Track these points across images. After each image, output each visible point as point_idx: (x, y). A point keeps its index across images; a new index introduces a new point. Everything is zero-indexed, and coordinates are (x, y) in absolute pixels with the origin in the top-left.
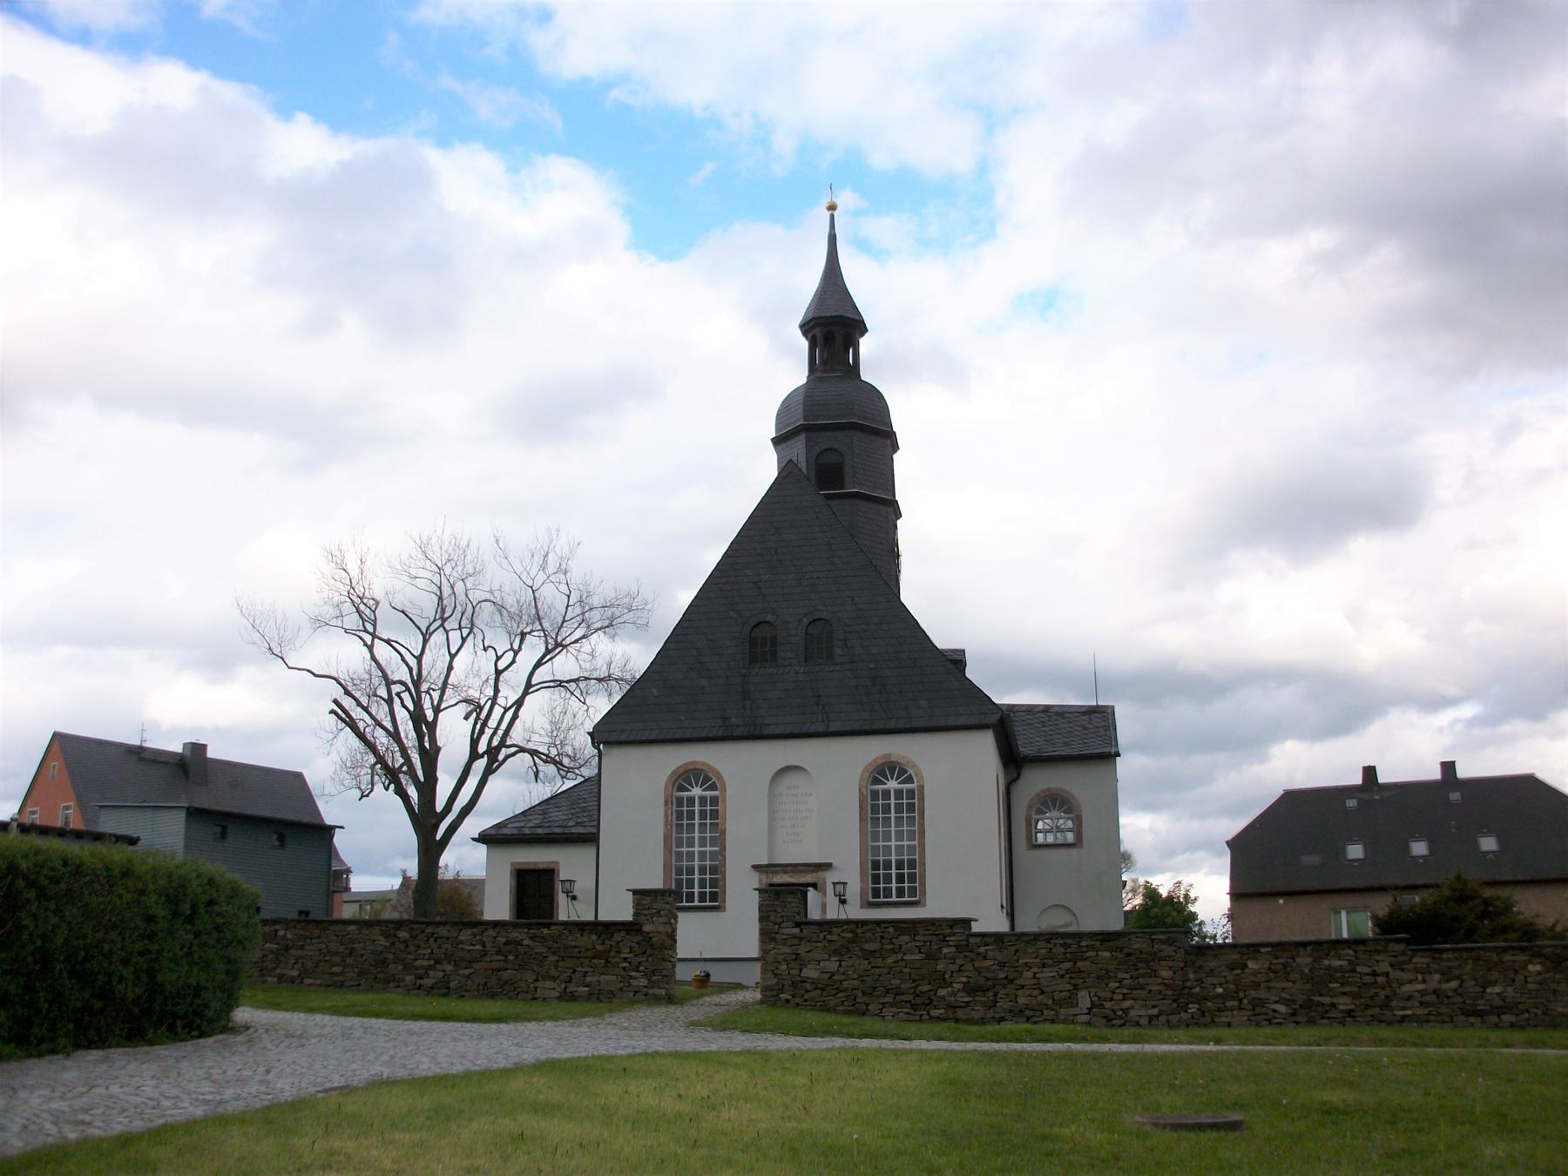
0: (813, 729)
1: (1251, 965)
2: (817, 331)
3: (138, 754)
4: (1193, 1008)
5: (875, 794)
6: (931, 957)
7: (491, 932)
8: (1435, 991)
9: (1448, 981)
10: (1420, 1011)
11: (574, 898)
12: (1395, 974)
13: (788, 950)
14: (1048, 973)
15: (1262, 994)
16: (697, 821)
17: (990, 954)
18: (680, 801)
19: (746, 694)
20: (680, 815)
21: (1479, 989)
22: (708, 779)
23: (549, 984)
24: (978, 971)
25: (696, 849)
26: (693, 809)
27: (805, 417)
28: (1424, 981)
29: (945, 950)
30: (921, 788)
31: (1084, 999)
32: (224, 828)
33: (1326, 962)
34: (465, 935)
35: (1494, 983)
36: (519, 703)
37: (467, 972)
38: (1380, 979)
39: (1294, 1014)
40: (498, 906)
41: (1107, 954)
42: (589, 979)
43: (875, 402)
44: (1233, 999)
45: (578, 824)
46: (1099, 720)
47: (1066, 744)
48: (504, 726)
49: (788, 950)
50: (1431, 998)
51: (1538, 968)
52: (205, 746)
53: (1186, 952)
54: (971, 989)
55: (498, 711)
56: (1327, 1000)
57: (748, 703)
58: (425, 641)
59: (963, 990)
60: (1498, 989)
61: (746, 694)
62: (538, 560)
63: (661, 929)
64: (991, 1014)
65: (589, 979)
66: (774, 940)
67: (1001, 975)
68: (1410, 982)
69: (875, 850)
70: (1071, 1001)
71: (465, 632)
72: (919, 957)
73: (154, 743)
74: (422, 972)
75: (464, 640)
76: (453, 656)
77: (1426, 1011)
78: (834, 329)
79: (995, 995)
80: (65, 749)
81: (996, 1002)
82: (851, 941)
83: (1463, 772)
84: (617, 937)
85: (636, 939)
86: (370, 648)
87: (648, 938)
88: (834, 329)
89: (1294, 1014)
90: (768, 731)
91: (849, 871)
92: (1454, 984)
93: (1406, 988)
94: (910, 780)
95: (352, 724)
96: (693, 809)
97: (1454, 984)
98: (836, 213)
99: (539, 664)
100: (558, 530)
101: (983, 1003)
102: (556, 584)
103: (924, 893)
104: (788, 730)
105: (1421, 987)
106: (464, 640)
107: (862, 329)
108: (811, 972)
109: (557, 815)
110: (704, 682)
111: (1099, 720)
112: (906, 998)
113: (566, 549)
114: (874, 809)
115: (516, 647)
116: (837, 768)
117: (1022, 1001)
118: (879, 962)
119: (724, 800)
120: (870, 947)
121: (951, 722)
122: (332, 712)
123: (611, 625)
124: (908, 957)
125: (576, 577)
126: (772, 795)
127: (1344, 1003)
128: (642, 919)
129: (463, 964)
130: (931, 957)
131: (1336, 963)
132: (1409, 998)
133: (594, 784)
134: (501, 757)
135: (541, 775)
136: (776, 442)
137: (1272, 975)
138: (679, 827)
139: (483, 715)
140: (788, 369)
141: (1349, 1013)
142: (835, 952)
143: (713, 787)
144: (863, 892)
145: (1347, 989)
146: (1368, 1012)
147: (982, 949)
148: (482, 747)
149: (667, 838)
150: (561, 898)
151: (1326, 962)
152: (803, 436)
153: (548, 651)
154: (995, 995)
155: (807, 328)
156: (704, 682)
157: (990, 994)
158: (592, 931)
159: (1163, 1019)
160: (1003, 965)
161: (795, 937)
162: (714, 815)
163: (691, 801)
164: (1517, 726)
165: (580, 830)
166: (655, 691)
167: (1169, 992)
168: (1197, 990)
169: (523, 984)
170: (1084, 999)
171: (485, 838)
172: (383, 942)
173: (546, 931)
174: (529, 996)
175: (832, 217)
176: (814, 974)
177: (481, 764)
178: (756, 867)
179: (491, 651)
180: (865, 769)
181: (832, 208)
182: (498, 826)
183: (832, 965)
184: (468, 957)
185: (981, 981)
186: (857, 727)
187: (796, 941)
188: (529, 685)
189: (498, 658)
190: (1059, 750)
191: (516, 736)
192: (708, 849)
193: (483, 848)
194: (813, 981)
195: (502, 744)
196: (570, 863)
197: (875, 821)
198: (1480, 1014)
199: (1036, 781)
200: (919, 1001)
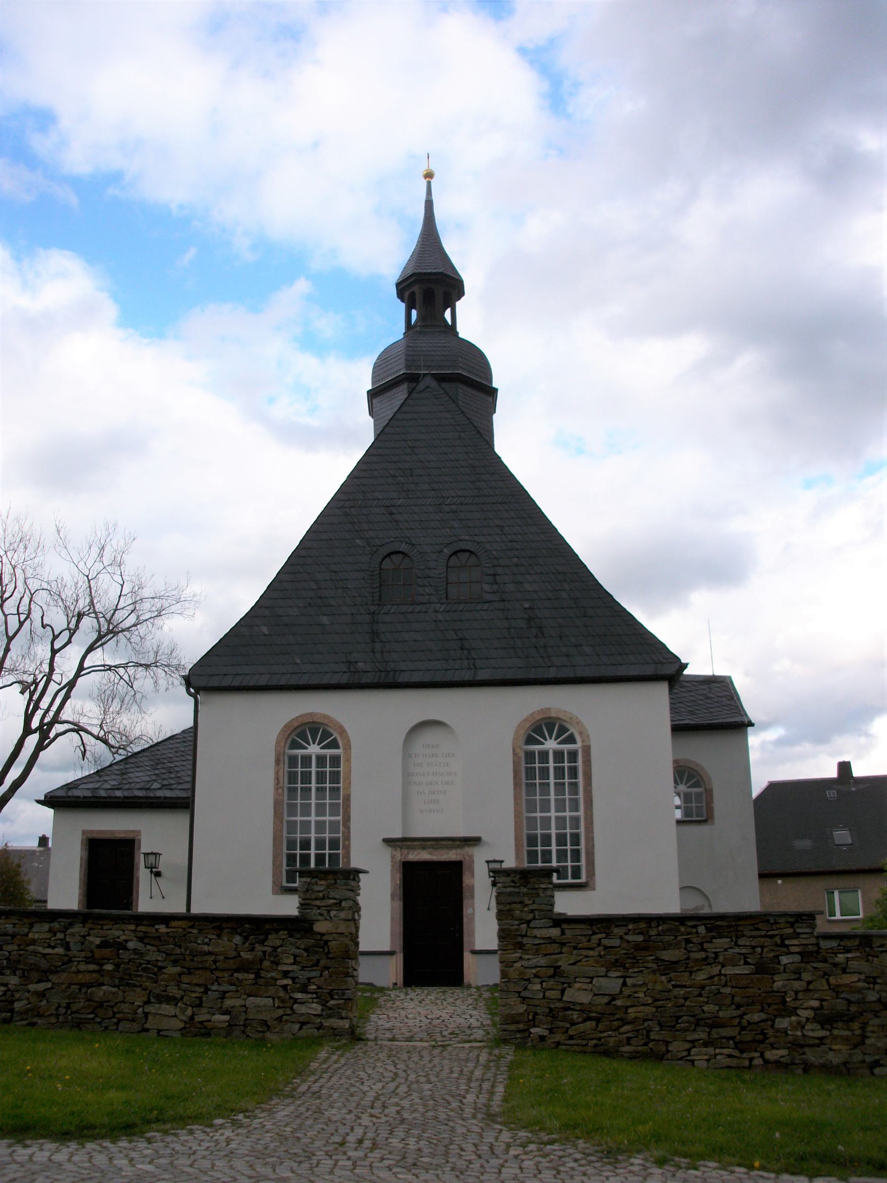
0: (457, 677)
2: (416, 289)
5: (530, 756)
6: (764, 969)
7: (78, 929)
11: (158, 874)
13: (542, 961)
16: (313, 785)
17: (854, 964)
18: (293, 760)
19: (375, 635)
20: (292, 778)
22: (326, 734)
24: (836, 990)
25: (313, 818)
26: (310, 767)
27: (408, 367)
29: (784, 960)
30: (587, 750)
34: (40, 931)
36: (71, 684)
37: (41, 987)
40: (64, 891)
42: (228, 1003)
43: (476, 360)
45: (163, 787)
47: (692, 713)
48: (54, 708)
49: (542, 961)
54: (825, 1019)
55: (53, 688)
57: (378, 646)
59: (815, 1019)
61: (375, 635)
62: (95, 551)
63: (342, 929)
64: (858, 1056)
65: (228, 1003)
66: (521, 946)
67: (872, 996)
69: (532, 822)
71: (23, 617)
72: (746, 970)
75: (21, 624)
76: (10, 639)
79: (863, 1027)
81: (864, 1037)
82: (637, 947)
83: (858, 771)
84: (274, 940)
85: (303, 943)
87: (322, 942)
90: (404, 678)
94: (571, 740)
96: (310, 767)
98: (433, 182)
99: (91, 649)
100: (115, 525)
101: (846, 1040)
102: (112, 574)
103: (591, 873)
104: (427, 678)
106: (21, 624)
108: (578, 994)
109: (140, 776)
110: (325, 620)
112: (724, 1032)
113: (122, 543)
114: (530, 771)
115: (72, 625)
116: (487, 723)
118: (685, 979)
119: (348, 760)
120: (669, 955)
121: (622, 671)
123: (159, 615)
124: (729, 971)
125: (129, 569)
126: (407, 755)
128: (313, 913)
129: (35, 975)
130: (764, 969)
133: (188, 740)
134: (52, 735)
135: (88, 754)
136: (372, 395)
138: (292, 791)
139: (35, 697)
142: (616, 964)
143: (334, 745)
147: (841, 958)
148: (35, 723)
149: (277, 804)
150: (143, 875)
153: (100, 637)
154: (863, 1027)
156: (325, 620)
157: (856, 1025)
158: (234, 931)
160: (871, 980)
161: (551, 940)
162: (335, 777)
163: (306, 760)
164: (807, 747)
165: (168, 793)
166: (265, 630)
169: (125, 1007)
171: (51, 801)
173: (163, 929)
174: (136, 1027)
175: (429, 184)
176: (585, 998)
177: (32, 740)
179: (48, 628)
180: (519, 726)
181: (429, 175)
182: (68, 786)
183: (612, 984)
184: (44, 964)
185: (840, 1005)
186: (510, 675)
187: (555, 948)
188: (81, 667)
189: (55, 637)
191: (65, 715)
192: (327, 818)
193: (50, 812)
194: (583, 1009)
195: (56, 720)
196: (155, 833)
197: (531, 787)
200: (747, 1036)
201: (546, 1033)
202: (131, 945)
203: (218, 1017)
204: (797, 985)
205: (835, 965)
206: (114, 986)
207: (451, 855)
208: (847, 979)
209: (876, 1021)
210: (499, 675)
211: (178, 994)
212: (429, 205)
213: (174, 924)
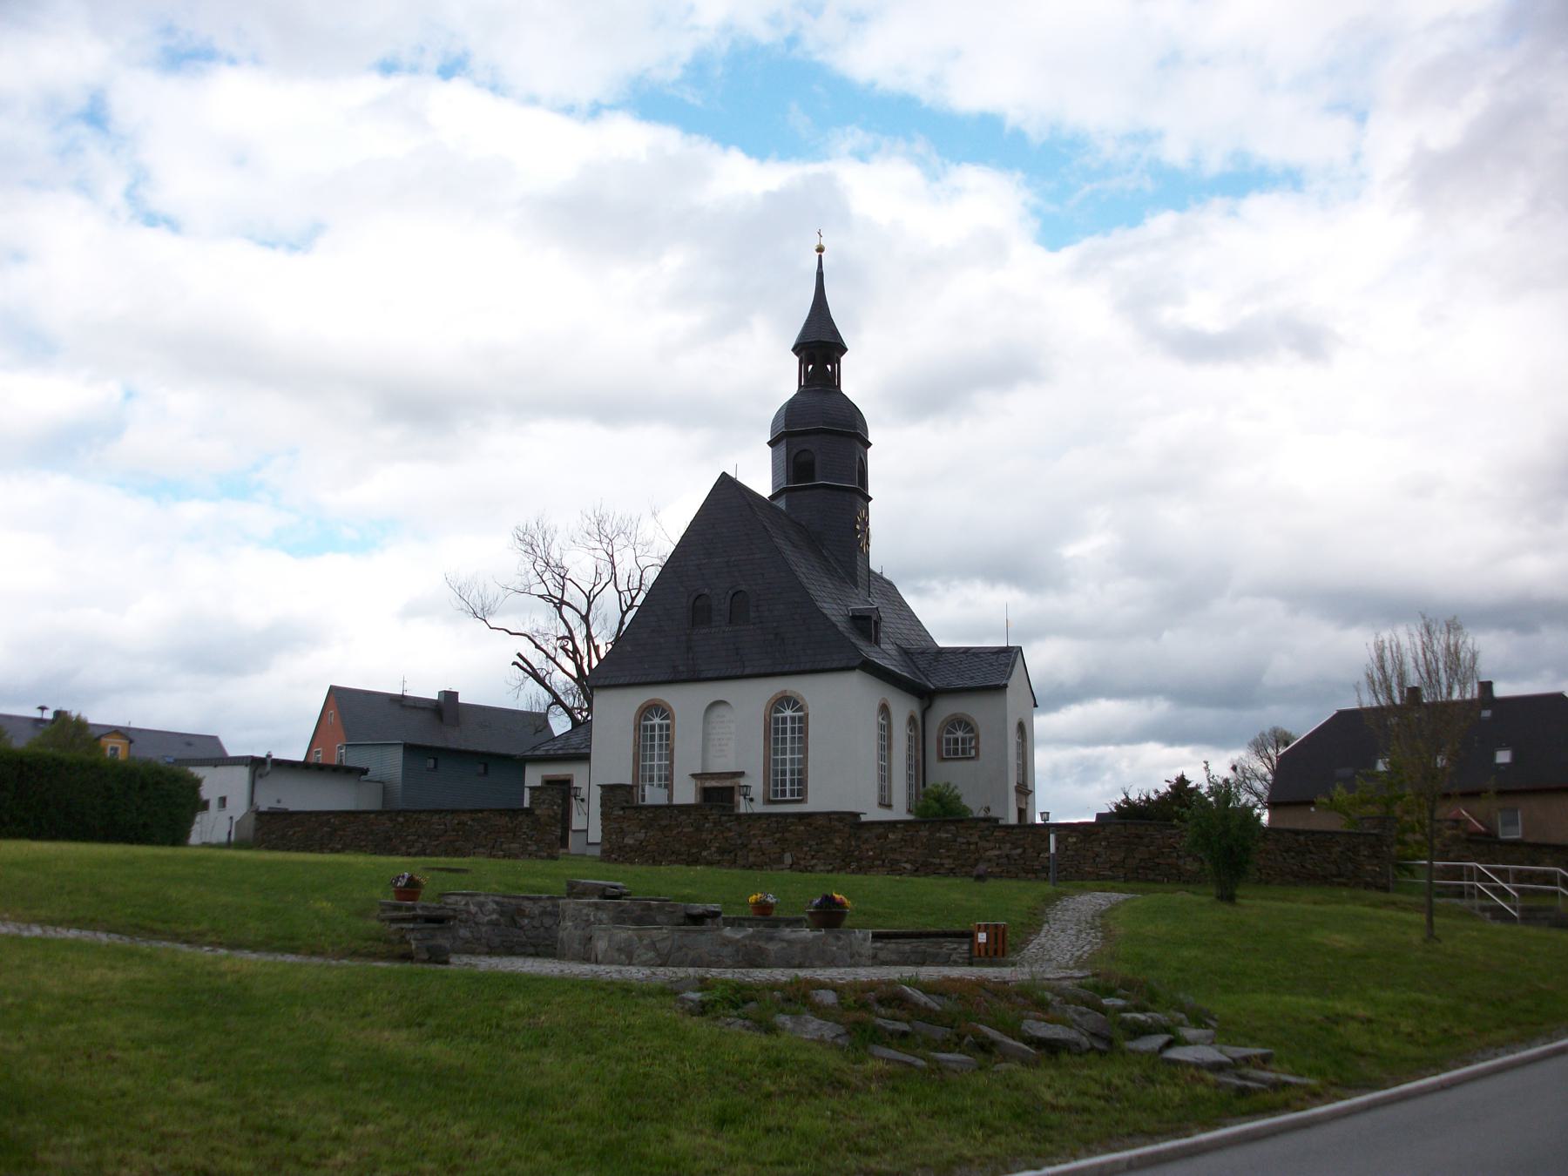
0: (733, 673)
3: (401, 702)
10: (997, 870)
12: (982, 844)
14: (767, 841)
15: (897, 857)
24: (726, 839)
25: (788, 756)
26: (652, 730)
31: (788, 859)
46: (1007, 658)
50: (1004, 860)
51: (468, 935)
52: (456, 694)
54: (721, 851)
58: (590, 604)
70: (780, 860)
73: (413, 692)
78: (820, 348)
80: (339, 698)
86: (559, 610)
88: (820, 348)
90: (703, 675)
91: (756, 782)
92: (1019, 851)
96: (652, 730)
97: (1019, 851)
107: (843, 350)
108: (629, 841)
111: (1007, 658)
114: (774, 732)
116: (749, 700)
117: (751, 859)
120: (664, 823)
121: (828, 665)
127: (948, 863)
136: (771, 444)
140: (786, 380)
143: (667, 718)
144: (766, 792)
155: (797, 349)
170: (788, 859)
172: (389, 824)
178: (694, 776)
181: (820, 250)
183: (641, 836)
190: (967, 689)
198: (1035, 872)
199: (945, 709)
207: (727, 783)
210: (756, 671)
212: (820, 275)
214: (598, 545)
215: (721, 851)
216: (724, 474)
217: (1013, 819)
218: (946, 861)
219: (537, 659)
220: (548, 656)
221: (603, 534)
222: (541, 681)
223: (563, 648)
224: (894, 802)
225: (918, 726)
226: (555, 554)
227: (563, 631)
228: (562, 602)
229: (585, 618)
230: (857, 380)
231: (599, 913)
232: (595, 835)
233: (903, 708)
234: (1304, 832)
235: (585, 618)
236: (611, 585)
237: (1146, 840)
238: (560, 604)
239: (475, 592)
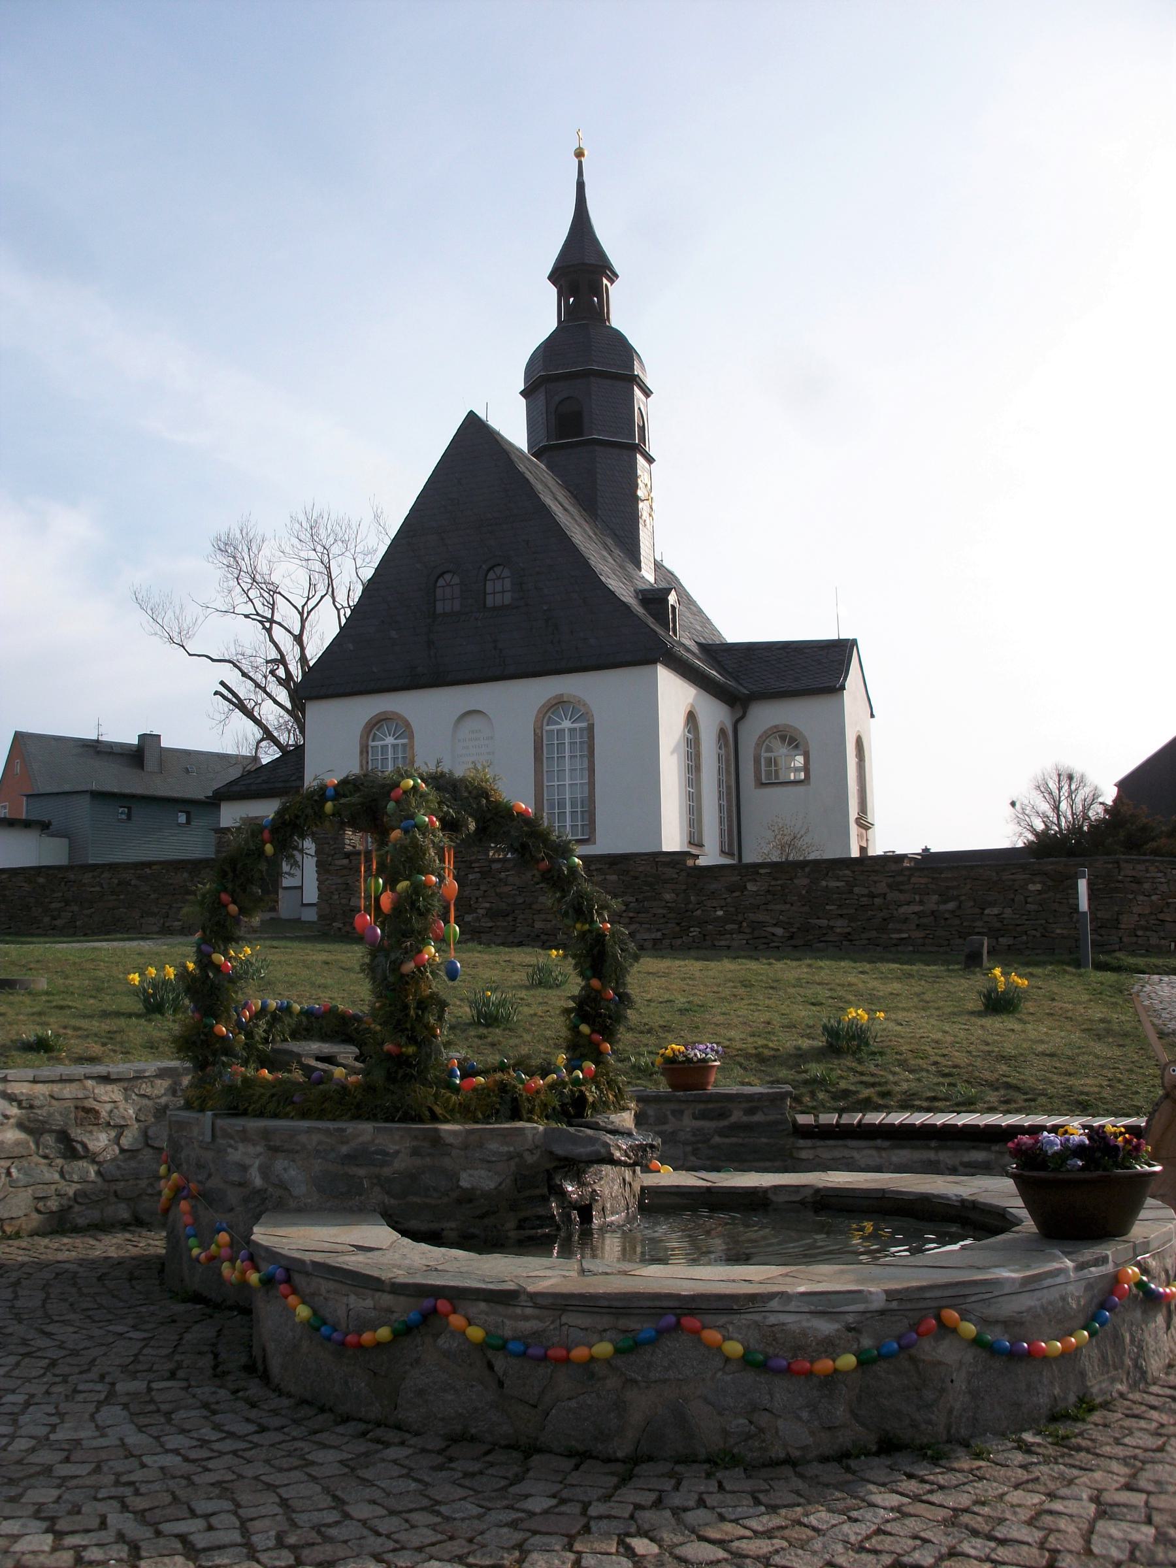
1: (751, 887)
4: (695, 932)
8: (933, 912)
9: (945, 902)
10: (918, 934)
12: (893, 896)
15: (761, 917)
21: (977, 910)
23: (152, 920)
28: (921, 902)
32: (129, 808)
33: (824, 883)
35: (992, 904)
37: (88, 912)
38: (877, 901)
39: (791, 938)
41: (614, 877)
44: (734, 922)
49: (339, 881)
51: (1038, 887)
53: (689, 875)
56: (824, 922)
58: (303, 622)
60: (996, 911)
67: (520, 900)
68: (909, 903)
74: (55, 913)
77: (922, 934)
78: (582, 272)
86: (269, 631)
88: (582, 272)
89: (791, 938)
92: (951, 905)
93: (902, 910)
95: (241, 706)
97: (951, 905)
105: (917, 908)
116: (513, 705)
122: (216, 693)
127: (841, 926)
131: (833, 884)
132: (906, 920)
137: (769, 897)
140: (542, 315)
141: (847, 936)
145: (845, 911)
146: (864, 936)
147: (503, 875)
151: (824, 883)
152: (543, 389)
154: (515, 919)
155: (554, 277)
157: (510, 918)
159: (666, 942)
161: (344, 867)
167: (672, 915)
168: (699, 912)
173: (148, 871)
175: (580, 163)
181: (579, 154)
199: (766, 716)
201: (341, 925)
202: (133, 882)
203: (176, 923)
204: (477, 893)
205: (500, 880)
206: (1051, 1512)
208: (506, 889)
209: (521, 916)
211: (156, 910)
212: (581, 186)
213: (154, 867)
214: (312, 555)
215: (491, 914)
216: (471, 412)
217: (855, 853)
218: (839, 922)
219: (244, 689)
220: (258, 685)
221: (317, 538)
222: (249, 714)
223: (272, 672)
224: (705, 843)
225: (730, 740)
226: (262, 567)
227: (274, 654)
228: (272, 621)
229: (299, 639)
230: (627, 310)
231: (280, 1164)
232: (311, 894)
233: (713, 714)
234: (126, 866)
235: (299, 639)
236: (328, 598)
237: (1147, 886)
238: (268, 624)
239: (170, 614)
